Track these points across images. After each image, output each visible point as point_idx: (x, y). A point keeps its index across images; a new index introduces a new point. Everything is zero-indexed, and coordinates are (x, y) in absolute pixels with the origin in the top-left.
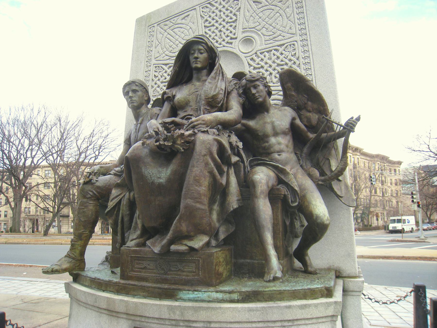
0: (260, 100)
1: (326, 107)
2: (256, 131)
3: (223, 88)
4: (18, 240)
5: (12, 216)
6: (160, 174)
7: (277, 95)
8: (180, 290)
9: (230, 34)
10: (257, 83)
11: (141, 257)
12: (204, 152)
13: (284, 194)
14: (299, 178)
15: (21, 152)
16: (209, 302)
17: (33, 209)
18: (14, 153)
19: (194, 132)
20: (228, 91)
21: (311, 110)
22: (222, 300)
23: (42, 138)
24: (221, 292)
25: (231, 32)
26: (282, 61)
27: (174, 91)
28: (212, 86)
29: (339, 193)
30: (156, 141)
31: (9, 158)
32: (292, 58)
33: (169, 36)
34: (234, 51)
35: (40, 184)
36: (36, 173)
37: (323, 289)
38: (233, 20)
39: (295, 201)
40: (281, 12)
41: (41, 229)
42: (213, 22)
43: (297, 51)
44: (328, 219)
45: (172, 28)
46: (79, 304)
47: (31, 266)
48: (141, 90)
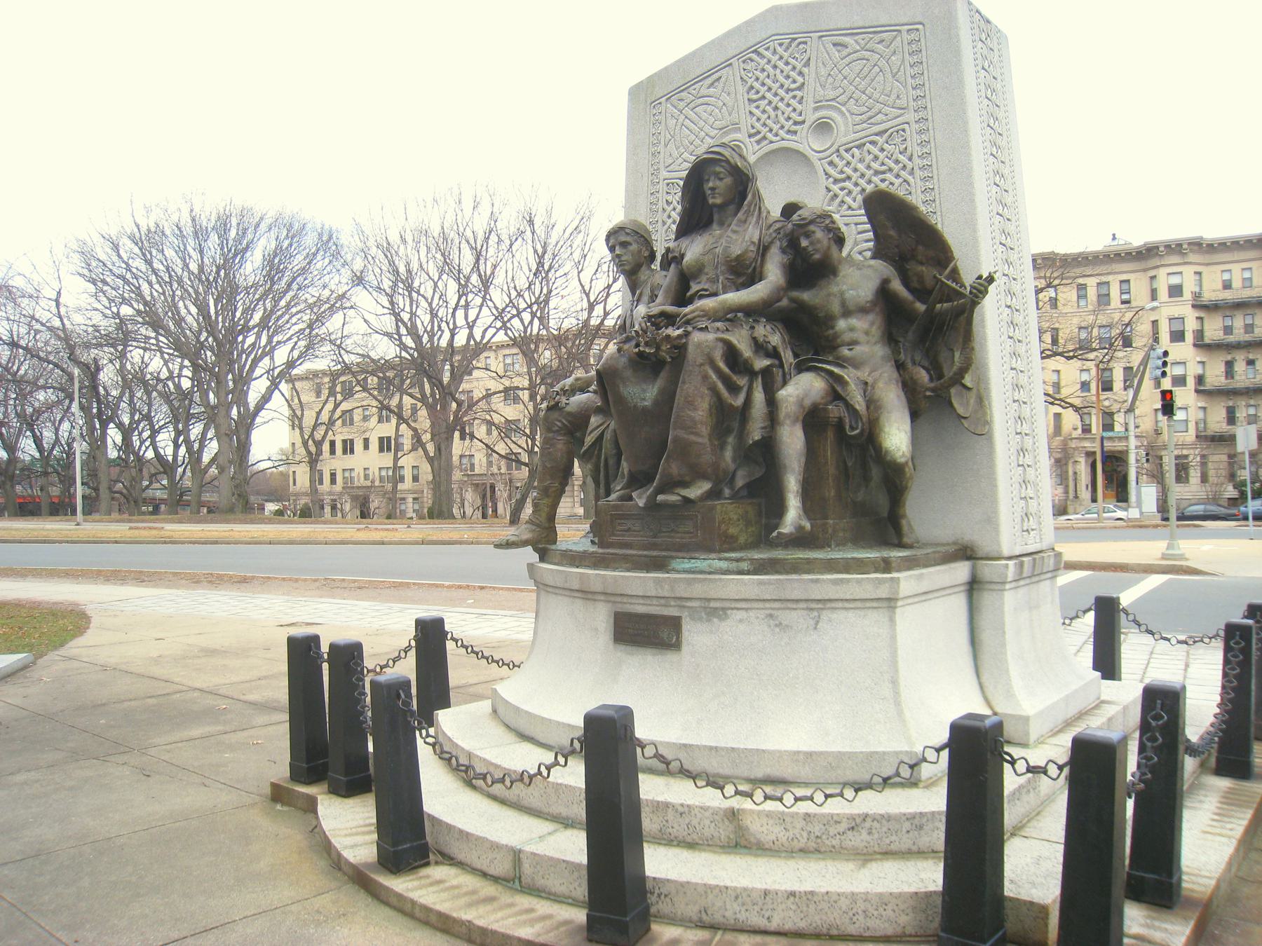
0: (817, 256)
2: (816, 308)
3: (756, 239)
4: (451, 535)
5: (430, 478)
6: (644, 394)
10: (812, 228)
12: (700, 360)
15: (440, 314)
16: (710, 573)
17: (480, 459)
18: (424, 318)
23: (488, 273)
24: (726, 559)
25: (794, 110)
26: (883, 164)
27: (684, 242)
28: (738, 238)
31: (413, 332)
32: (901, 157)
33: (687, 122)
34: (800, 147)
35: (495, 393)
36: (479, 365)
40: (882, 63)
41: (504, 509)
43: (909, 143)
45: (692, 105)
47: (482, 588)
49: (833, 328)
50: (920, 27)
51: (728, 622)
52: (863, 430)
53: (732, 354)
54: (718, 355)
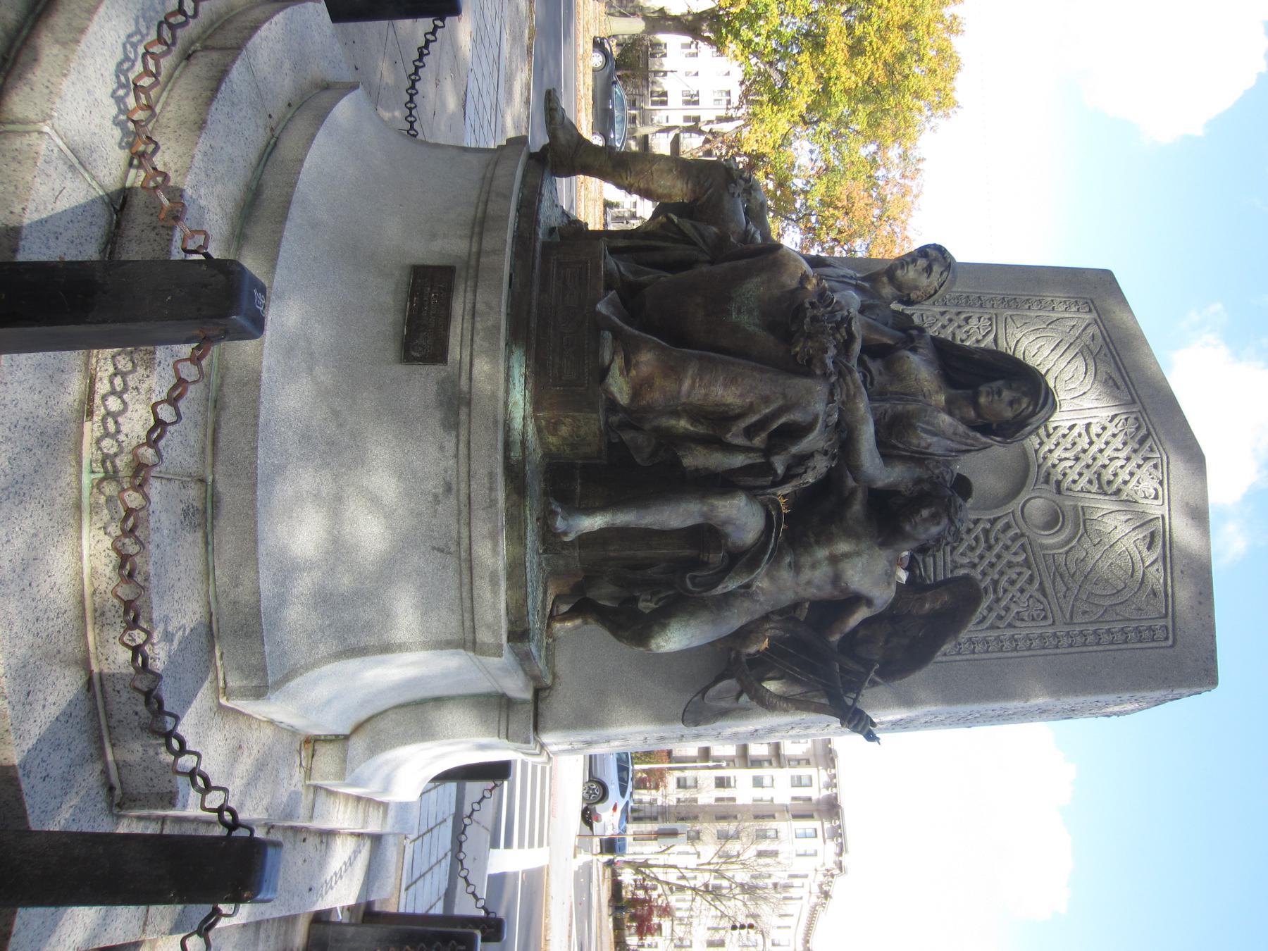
0: (908, 528)
6: (745, 318)
10: (945, 521)
19: (831, 374)
26: (1005, 591)
27: (926, 351)
28: (941, 425)
29: (712, 692)
30: (812, 304)
38: (1105, 487)
39: (694, 585)
44: (659, 647)
46: (488, 165)
48: (931, 283)
49: (818, 542)
50: (1170, 642)
51: (440, 431)
52: (692, 592)
53: (795, 432)
54: (796, 416)
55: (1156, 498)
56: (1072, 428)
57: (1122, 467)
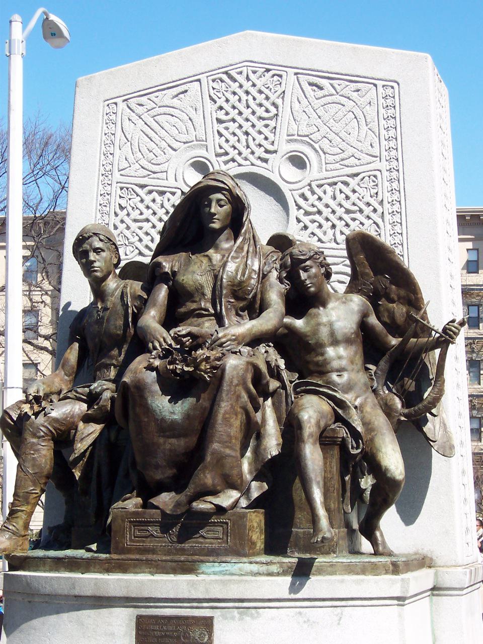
1: (419, 296)
7: (341, 271)
8: (202, 562)
9: (264, 143)
11: (144, 522)
13: (342, 436)
14: (366, 412)
20: (263, 274)
21: (396, 298)
22: (257, 573)
25: (266, 138)
32: (372, 201)
37: (388, 563)
38: (271, 115)
42: (233, 113)
44: (401, 474)
45: (152, 113)
49: (322, 354)
52: (363, 449)
55: (280, 76)
56: (221, 135)
57: (254, 99)
